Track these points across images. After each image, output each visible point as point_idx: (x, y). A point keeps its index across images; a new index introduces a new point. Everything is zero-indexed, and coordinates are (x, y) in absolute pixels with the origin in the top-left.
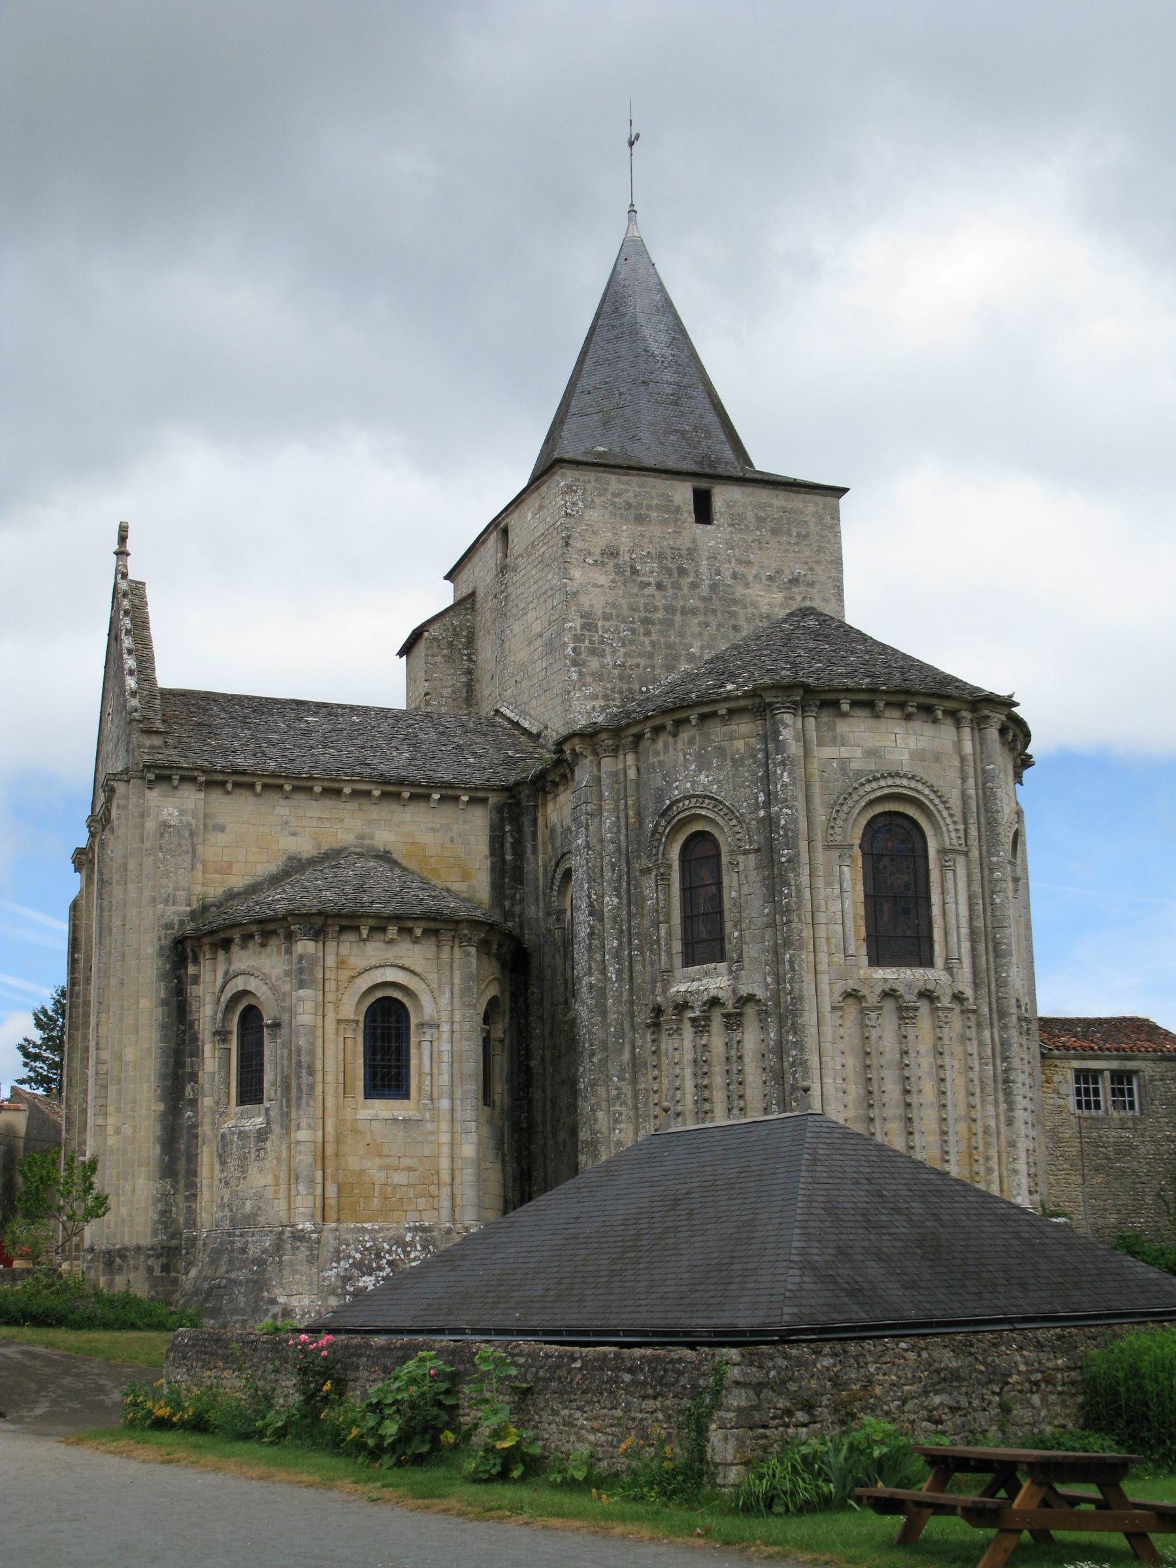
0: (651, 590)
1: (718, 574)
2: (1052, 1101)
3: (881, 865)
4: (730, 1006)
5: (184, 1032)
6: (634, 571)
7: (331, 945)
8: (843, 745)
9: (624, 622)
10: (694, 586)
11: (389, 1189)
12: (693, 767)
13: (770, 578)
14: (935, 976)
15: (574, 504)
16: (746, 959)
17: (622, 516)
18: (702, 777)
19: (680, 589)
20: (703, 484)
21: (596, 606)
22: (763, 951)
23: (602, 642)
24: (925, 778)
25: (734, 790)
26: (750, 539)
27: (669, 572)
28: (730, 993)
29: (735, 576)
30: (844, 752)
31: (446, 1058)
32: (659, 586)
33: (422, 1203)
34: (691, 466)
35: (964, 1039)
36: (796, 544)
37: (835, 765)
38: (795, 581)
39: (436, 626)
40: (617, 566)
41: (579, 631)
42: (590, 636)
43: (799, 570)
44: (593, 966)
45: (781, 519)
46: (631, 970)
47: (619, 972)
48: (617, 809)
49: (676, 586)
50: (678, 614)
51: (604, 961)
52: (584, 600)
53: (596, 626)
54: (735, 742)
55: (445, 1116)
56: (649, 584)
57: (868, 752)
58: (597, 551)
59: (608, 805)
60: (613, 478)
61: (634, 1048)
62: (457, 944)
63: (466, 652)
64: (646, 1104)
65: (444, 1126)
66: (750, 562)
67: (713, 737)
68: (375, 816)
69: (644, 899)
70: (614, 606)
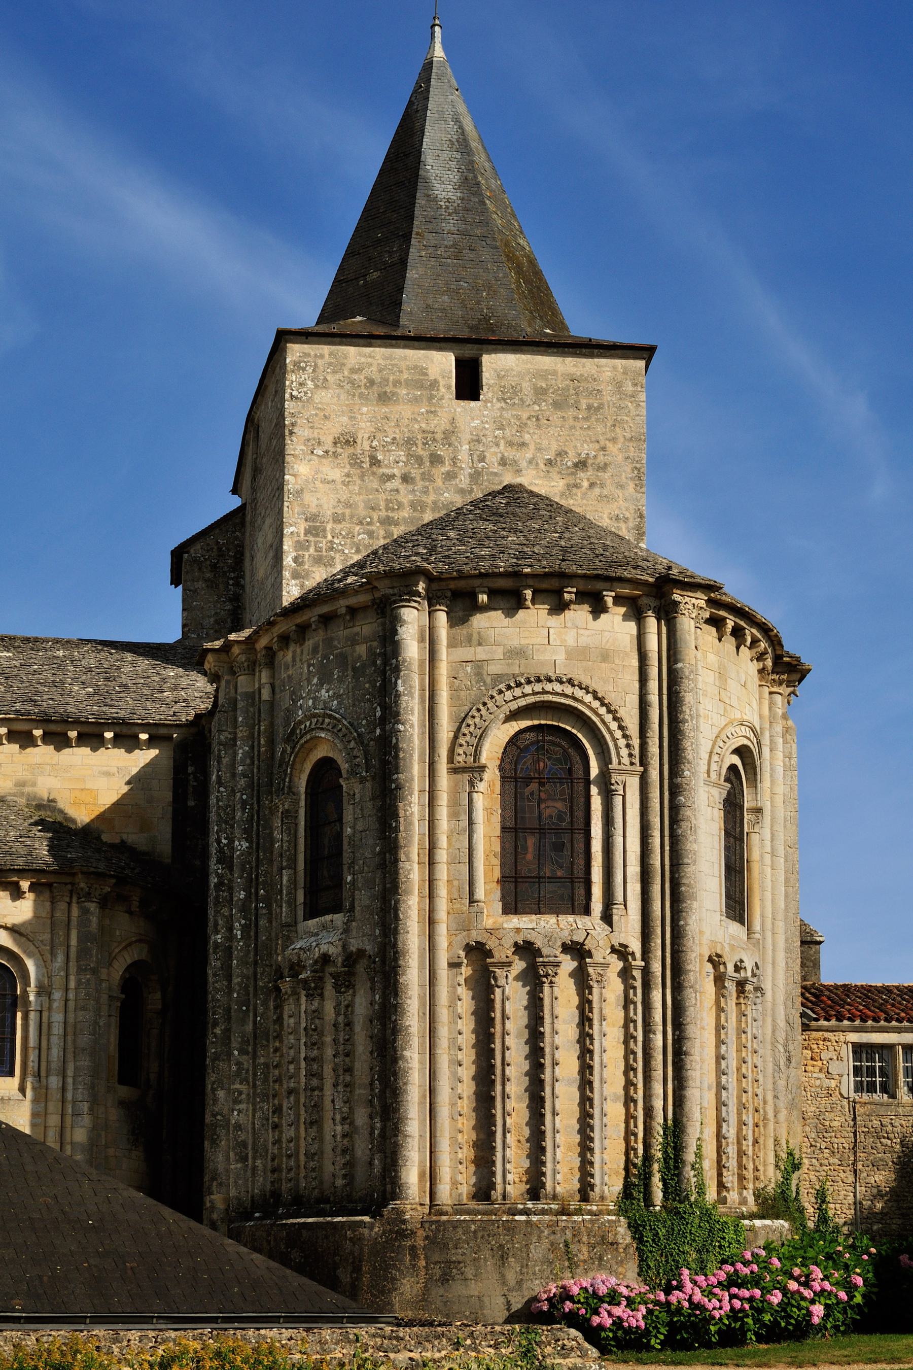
0: (396, 483)
1: (482, 459)
2: (818, 1082)
3: (527, 791)
4: (339, 964)
6: (375, 462)
8: (480, 644)
9: (361, 523)
10: (450, 476)
12: (315, 681)
13: (549, 463)
14: (588, 927)
15: (301, 384)
16: (357, 908)
17: (361, 396)
18: (323, 691)
19: (432, 480)
20: (468, 351)
21: (325, 506)
23: (332, 549)
24: (586, 681)
25: (354, 705)
26: (525, 416)
27: (419, 460)
28: (340, 948)
29: (503, 462)
30: (481, 653)
31: (57, 1029)
32: (406, 479)
34: (465, 333)
36: (586, 419)
37: (469, 669)
38: (581, 465)
39: (198, 546)
40: (353, 457)
41: (302, 537)
42: (316, 543)
43: (587, 450)
44: (220, 922)
45: (567, 388)
46: (257, 925)
47: (244, 928)
48: (251, 736)
49: (427, 477)
50: (428, 511)
51: (231, 915)
52: (310, 500)
53: (324, 530)
54: (357, 647)
56: (393, 476)
57: (510, 651)
58: (328, 440)
59: (242, 732)
60: (351, 351)
61: (255, 1016)
62: (74, 900)
63: (232, 575)
64: (266, 1080)
66: (523, 444)
67: (336, 643)
69: (272, 841)
70: (348, 505)
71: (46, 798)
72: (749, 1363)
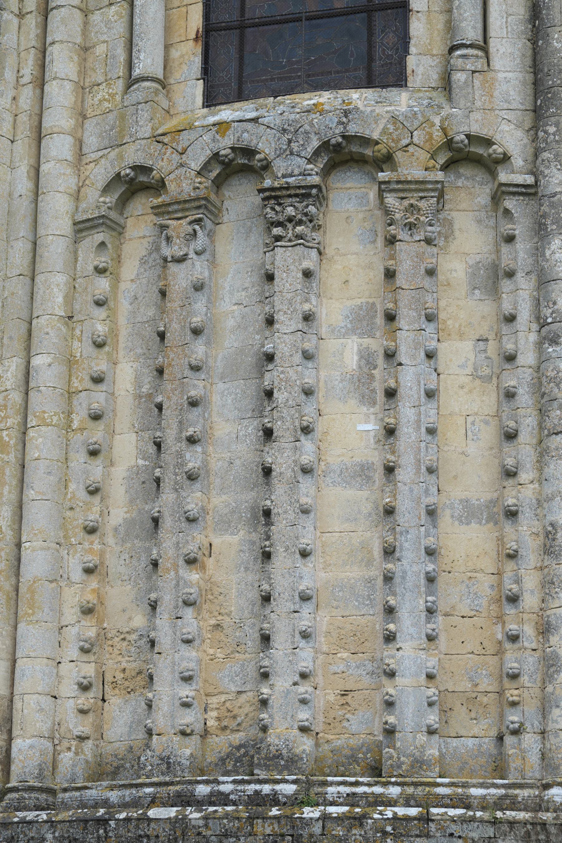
5: (150, 591)
22: (49, 169)
35: (496, 276)
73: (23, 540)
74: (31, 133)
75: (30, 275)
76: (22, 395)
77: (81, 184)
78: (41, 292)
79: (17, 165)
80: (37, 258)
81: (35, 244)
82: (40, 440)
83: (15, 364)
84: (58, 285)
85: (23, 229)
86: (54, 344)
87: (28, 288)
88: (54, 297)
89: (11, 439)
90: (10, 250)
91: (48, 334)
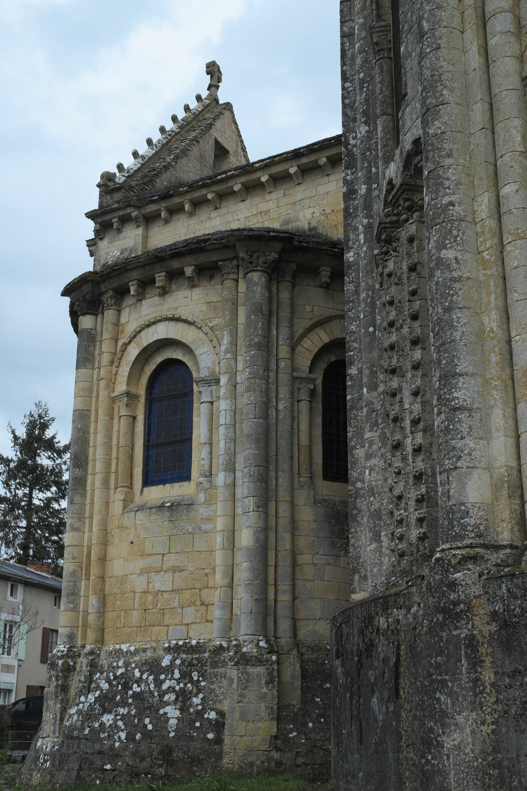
7: (110, 314)
11: (150, 597)
31: (224, 418)
33: (190, 614)
55: (221, 494)
65: (220, 508)
68: (300, 196)
71: (307, 227)
72: (404, 79)
73: (513, 334)
74: (477, 21)
75: (490, 127)
76: (496, 222)
77: (523, 50)
78: (502, 137)
79: (469, 48)
80: (495, 112)
81: (491, 104)
82: (518, 251)
83: (487, 198)
84: (516, 128)
85: (478, 94)
86: (518, 174)
87: (490, 138)
88: (513, 138)
89: (492, 256)
90: (471, 113)
91: (512, 167)
